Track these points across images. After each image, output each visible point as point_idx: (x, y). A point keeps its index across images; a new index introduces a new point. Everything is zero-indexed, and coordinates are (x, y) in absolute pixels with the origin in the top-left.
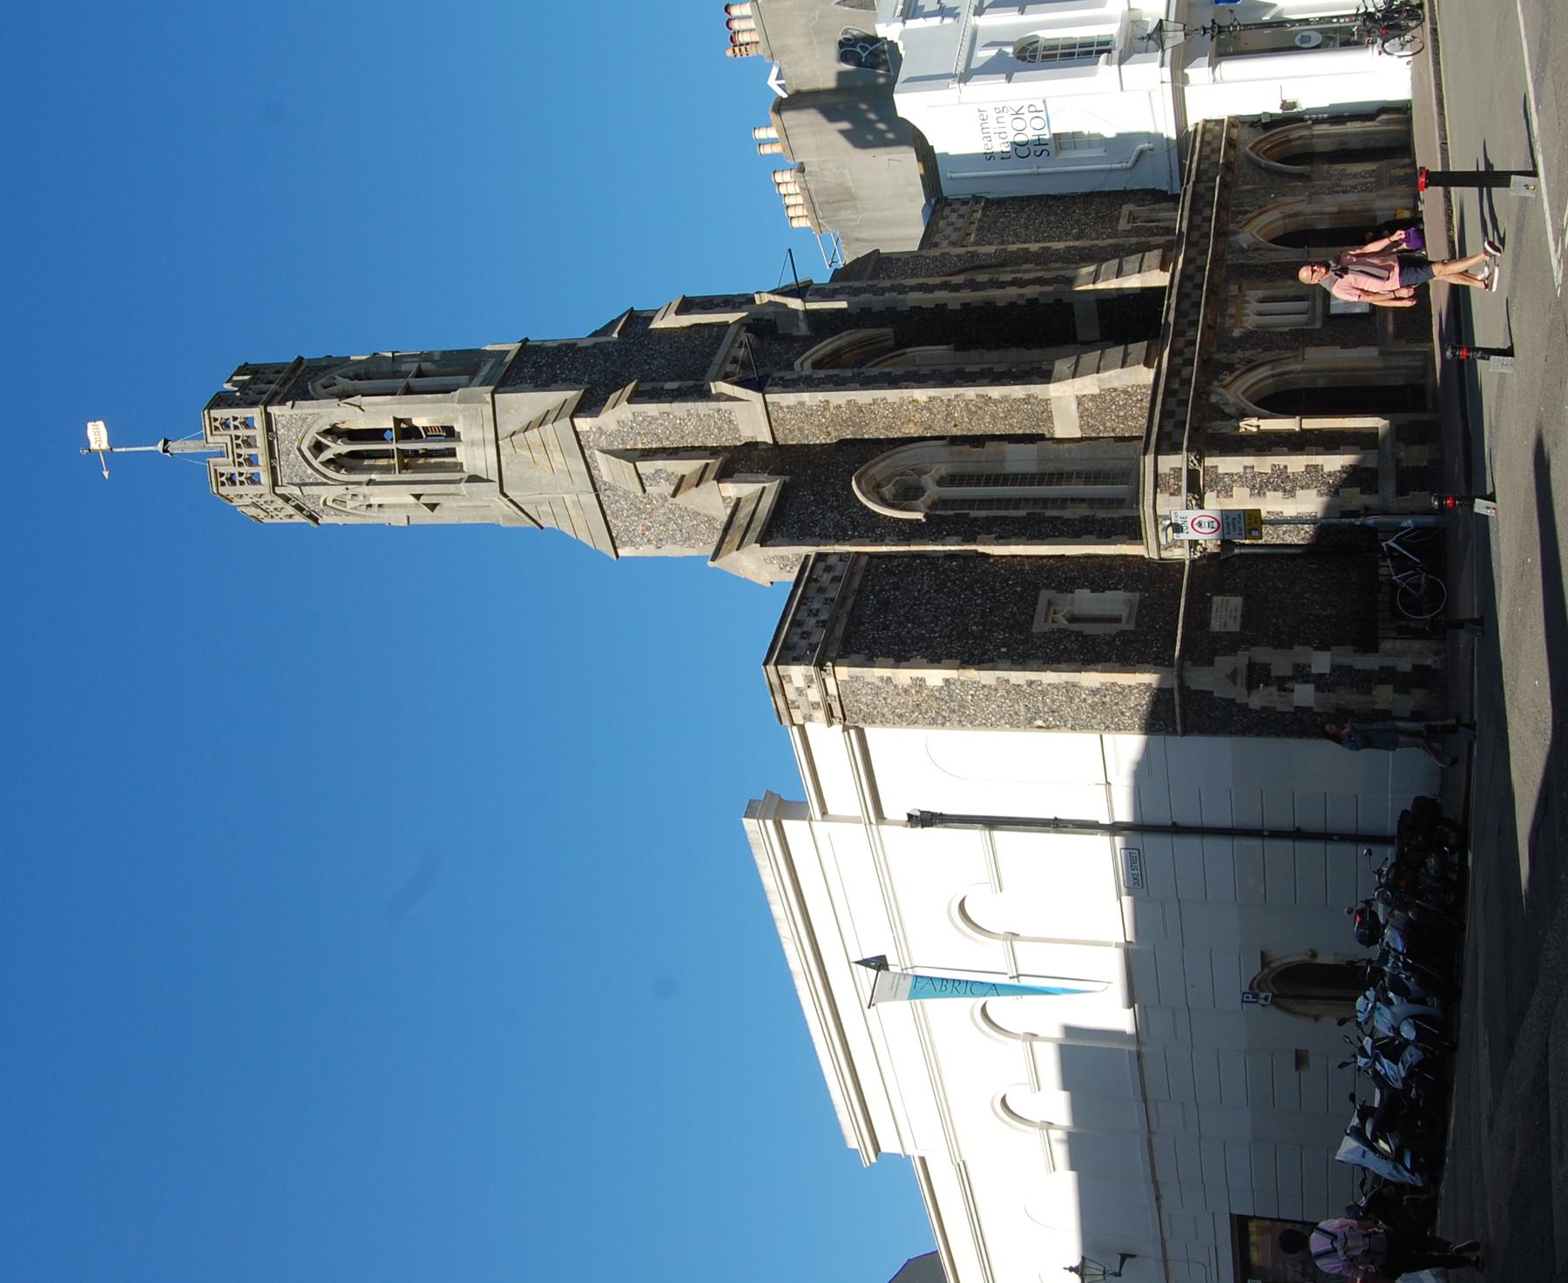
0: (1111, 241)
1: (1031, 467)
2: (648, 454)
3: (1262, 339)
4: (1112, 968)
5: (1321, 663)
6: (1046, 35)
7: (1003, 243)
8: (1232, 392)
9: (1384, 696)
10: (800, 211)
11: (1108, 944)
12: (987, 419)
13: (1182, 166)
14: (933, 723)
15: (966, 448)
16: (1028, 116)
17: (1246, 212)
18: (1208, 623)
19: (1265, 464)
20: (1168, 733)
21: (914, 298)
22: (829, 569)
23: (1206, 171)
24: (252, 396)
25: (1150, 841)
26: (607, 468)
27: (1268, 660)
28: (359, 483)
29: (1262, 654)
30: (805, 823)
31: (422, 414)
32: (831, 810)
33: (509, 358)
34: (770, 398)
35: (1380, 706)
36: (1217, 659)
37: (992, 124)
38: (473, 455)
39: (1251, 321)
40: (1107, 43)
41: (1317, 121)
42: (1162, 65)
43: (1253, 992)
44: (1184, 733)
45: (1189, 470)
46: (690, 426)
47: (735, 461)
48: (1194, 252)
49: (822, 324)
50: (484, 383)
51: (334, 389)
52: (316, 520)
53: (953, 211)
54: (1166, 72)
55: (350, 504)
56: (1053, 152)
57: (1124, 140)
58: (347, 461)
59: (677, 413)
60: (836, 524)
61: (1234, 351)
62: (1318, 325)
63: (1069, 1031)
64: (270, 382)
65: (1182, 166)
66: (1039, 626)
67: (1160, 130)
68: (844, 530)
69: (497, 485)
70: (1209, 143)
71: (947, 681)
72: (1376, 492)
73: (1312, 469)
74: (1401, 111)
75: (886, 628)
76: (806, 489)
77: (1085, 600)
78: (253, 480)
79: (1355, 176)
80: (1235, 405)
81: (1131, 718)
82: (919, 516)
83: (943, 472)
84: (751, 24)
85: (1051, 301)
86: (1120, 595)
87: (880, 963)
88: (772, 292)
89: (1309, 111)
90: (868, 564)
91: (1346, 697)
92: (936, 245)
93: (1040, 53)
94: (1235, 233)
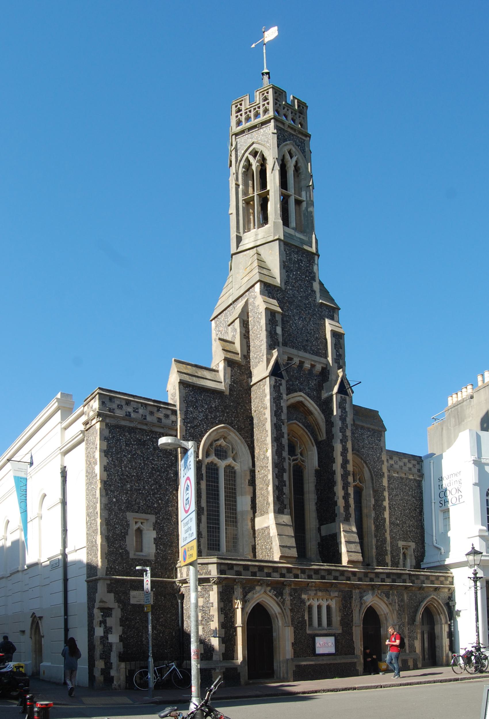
0: (388, 539)
5: (114, 638)
9: (100, 664)
11: (40, 556)
12: (261, 486)
15: (248, 477)
16: (457, 495)
21: (338, 448)
22: (167, 416)
24: (282, 112)
27: (113, 616)
28: (237, 179)
29: (117, 613)
30: (59, 420)
35: (96, 663)
36: (112, 595)
44: (88, 582)
45: (209, 578)
46: (257, 343)
47: (239, 368)
49: (326, 406)
57: (446, 541)
60: (194, 418)
61: (291, 595)
62: (308, 632)
66: (130, 516)
69: (235, 251)
71: (96, 475)
75: (127, 445)
77: (150, 535)
78: (239, 123)
83: (236, 468)
87: (31, 464)
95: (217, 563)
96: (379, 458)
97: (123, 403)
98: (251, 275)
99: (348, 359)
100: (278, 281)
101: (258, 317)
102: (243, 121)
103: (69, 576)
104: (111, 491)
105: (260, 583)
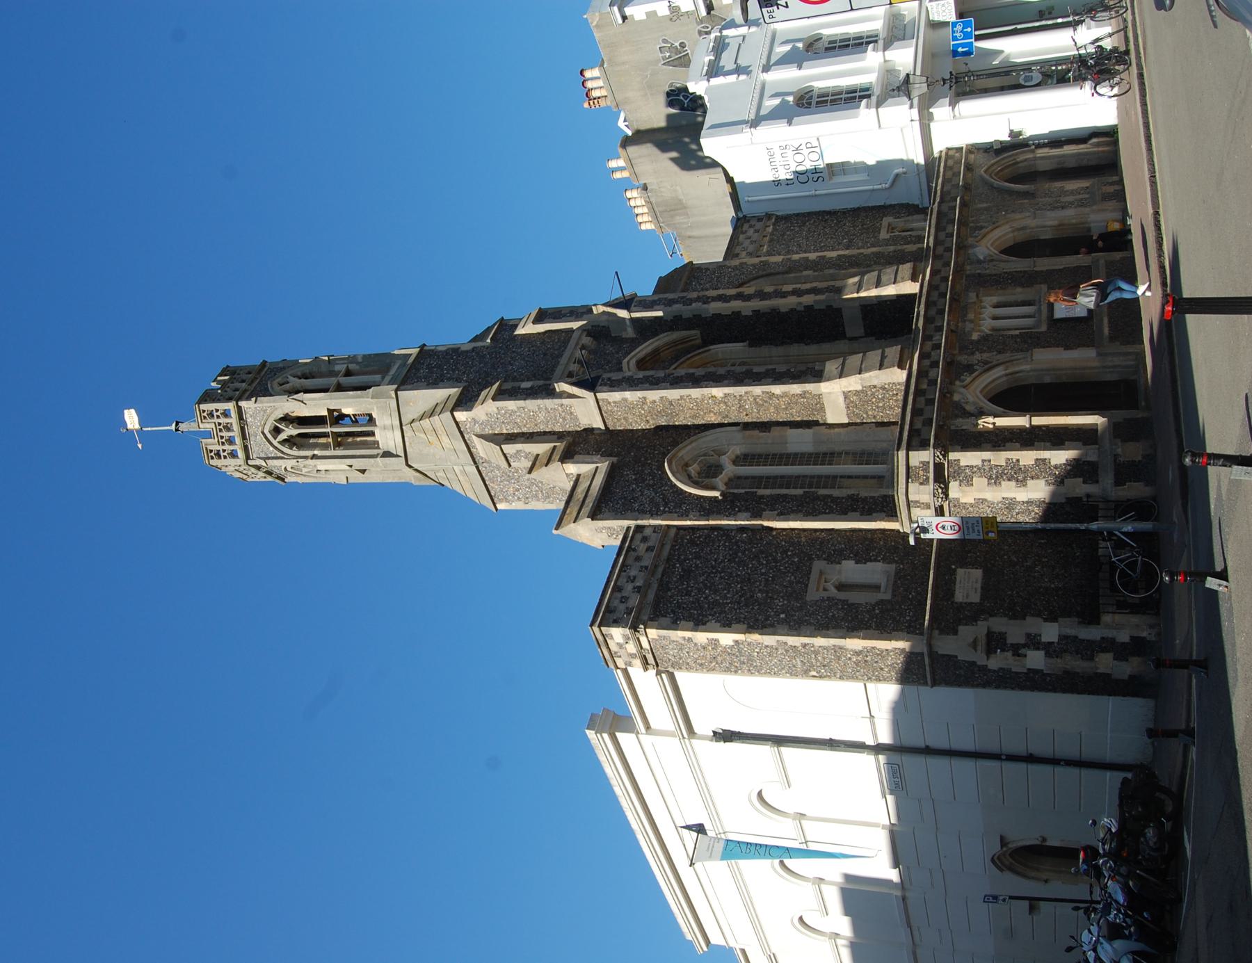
0: (874, 249)
1: (808, 448)
2: (511, 438)
3: (997, 342)
4: (879, 844)
5: (1050, 632)
6: (819, 85)
7: (788, 252)
8: (972, 391)
10: (646, 218)
11: (876, 825)
12: (772, 409)
13: (929, 188)
14: (728, 670)
15: (756, 433)
16: (805, 152)
17: (982, 228)
18: (953, 595)
19: (1000, 458)
20: (920, 684)
21: (716, 307)
22: (645, 539)
23: (949, 193)
24: (230, 393)
25: (908, 761)
26: (481, 448)
27: (1004, 630)
29: (999, 624)
30: (633, 736)
31: (348, 406)
32: (653, 725)
33: (411, 360)
34: (599, 395)
35: (1102, 670)
36: (961, 628)
37: (778, 158)
38: (387, 437)
39: (987, 325)
40: (868, 89)
41: (1039, 146)
42: (911, 107)
43: (999, 862)
46: (541, 416)
47: (575, 444)
48: (939, 264)
49: (645, 329)
50: (390, 383)
51: (287, 386)
52: (283, 480)
53: (751, 226)
54: (915, 113)
55: (305, 470)
56: (827, 178)
57: (883, 166)
58: (298, 440)
59: (531, 408)
60: (652, 501)
61: (973, 353)
62: (1044, 328)
63: (848, 878)
64: (243, 381)
65: (929, 188)
66: (813, 595)
67: (911, 157)
68: (657, 506)
69: (403, 459)
70: (951, 168)
71: (736, 642)
72: (1097, 482)
73: (1041, 462)
74: (1109, 134)
75: (688, 594)
76: (630, 469)
77: (850, 570)
78: (233, 455)
79: (1072, 192)
80: (974, 403)
81: (889, 672)
82: (716, 494)
83: (738, 452)
84: (600, 83)
85: (823, 307)
86: (878, 567)
87: (700, 829)
88: (604, 305)
89: (1032, 138)
90: (677, 534)
91: (1074, 663)
92: (737, 255)
93: (815, 100)
94: (973, 246)
95: (908, 450)
96: (735, 268)
97: (619, 595)
98: (440, 430)
99: (577, 302)
100: (454, 391)
101: (503, 415)
102: (232, 448)
103: (921, 744)
104: (767, 619)
105: (946, 394)
